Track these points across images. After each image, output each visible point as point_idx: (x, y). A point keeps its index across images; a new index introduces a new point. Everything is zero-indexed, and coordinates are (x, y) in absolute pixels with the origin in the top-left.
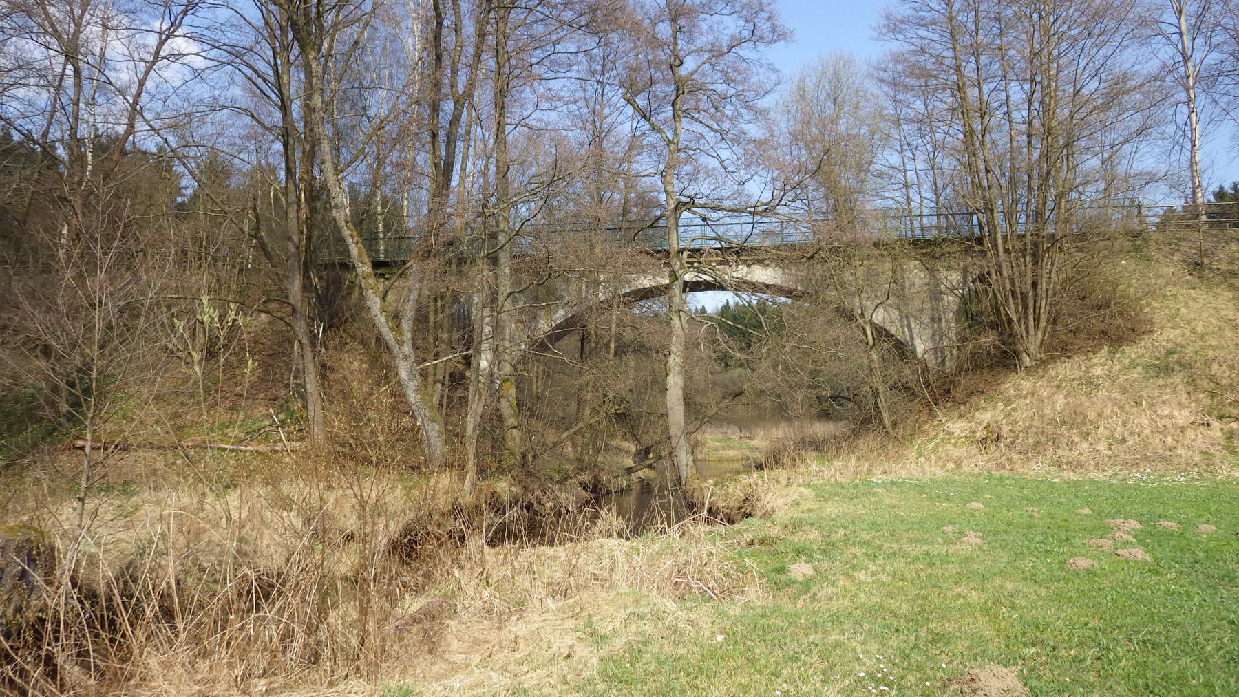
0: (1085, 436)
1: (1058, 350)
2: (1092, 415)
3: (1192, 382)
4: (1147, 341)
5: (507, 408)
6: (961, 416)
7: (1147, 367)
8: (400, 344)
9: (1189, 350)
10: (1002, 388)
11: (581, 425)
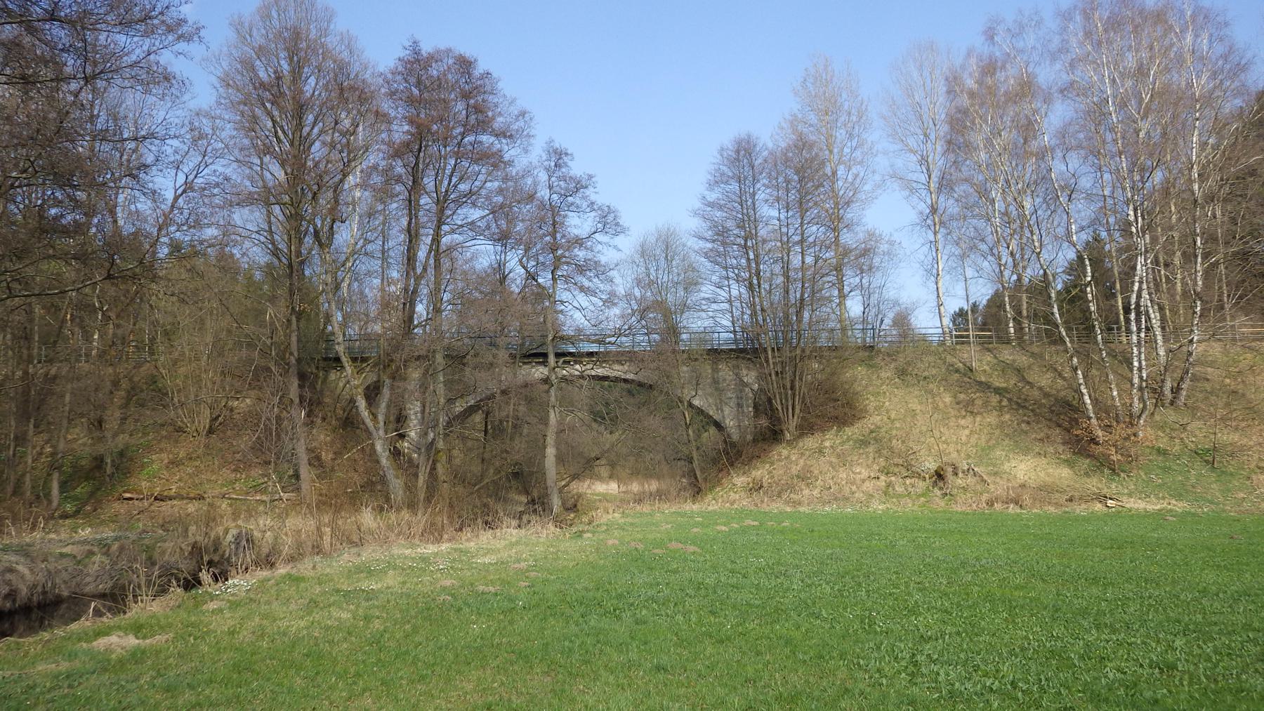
1: (807, 429)
2: (816, 472)
3: (878, 451)
4: (858, 425)
7: (856, 442)
8: (377, 429)
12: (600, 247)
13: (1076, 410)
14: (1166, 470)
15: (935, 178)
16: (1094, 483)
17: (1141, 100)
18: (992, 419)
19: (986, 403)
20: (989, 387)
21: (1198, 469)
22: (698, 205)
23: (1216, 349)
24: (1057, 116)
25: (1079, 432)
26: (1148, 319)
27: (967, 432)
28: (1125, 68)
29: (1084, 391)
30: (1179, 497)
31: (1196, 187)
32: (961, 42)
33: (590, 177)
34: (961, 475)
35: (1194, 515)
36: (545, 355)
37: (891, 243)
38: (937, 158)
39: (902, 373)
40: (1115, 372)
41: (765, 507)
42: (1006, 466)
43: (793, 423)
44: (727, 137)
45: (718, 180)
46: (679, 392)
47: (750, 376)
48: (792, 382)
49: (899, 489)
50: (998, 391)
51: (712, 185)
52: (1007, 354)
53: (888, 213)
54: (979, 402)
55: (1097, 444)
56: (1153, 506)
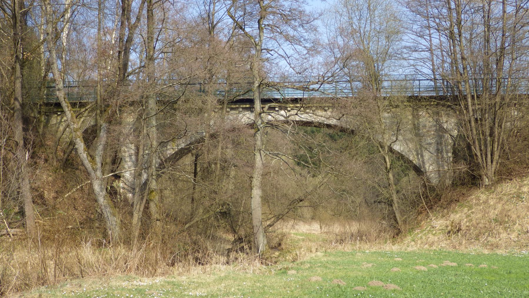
0: (505, 229)
1: (505, 174)
2: (514, 216)
6: (443, 216)
8: (95, 170)
10: (469, 199)
11: (197, 219)
36: (251, 101)
46: (379, 137)
47: (450, 123)
48: (492, 129)
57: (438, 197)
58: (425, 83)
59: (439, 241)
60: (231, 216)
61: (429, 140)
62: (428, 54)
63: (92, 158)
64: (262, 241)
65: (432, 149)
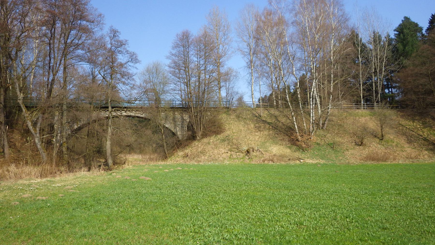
1: (205, 135)
2: (207, 150)
3: (228, 143)
4: (222, 134)
5: (64, 149)
7: (221, 140)
8: (36, 134)
9: (230, 136)
12: (130, 67)
13: (293, 130)
14: (319, 150)
15: (252, 51)
16: (297, 154)
17: (316, 28)
18: (266, 133)
19: (264, 128)
20: (266, 122)
21: (329, 150)
22: (168, 54)
23: (336, 112)
24: (290, 31)
25: (293, 137)
26: (316, 100)
27: (258, 137)
28: (312, 17)
29: (295, 124)
30: (322, 159)
31: (332, 58)
32: (261, 4)
33: (126, 41)
34: (255, 151)
35: (327, 164)
36: (108, 107)
37: (237, 72)
38: (253, 44)
39: (238, 117)
40: (305, 117)
41: (188, 163)
42: (270, 149)
43: (200, 133)
44: (180, 31)
45: (176, 46)
46: (160, 121)
47: (186, 117)
48: (200, 119)
49: (234, 156)
50: (269, 123)
51: (173, 48)
52: (273, 111)
53: (236, 62)
54: (262, 127)
55: (299, 141)
56: (315, 162)
57: (181, 144)
58: (177, 102)
59: (180, 160)
60: (100, 152)
61: (178, 123)
62: (180, 92)
63: (35, 130)
64: (8, 177)
65: (180, 126)
